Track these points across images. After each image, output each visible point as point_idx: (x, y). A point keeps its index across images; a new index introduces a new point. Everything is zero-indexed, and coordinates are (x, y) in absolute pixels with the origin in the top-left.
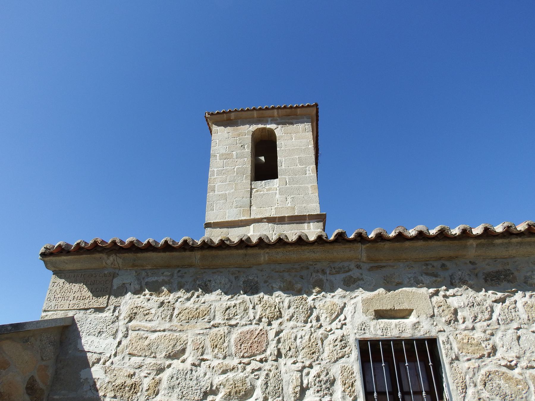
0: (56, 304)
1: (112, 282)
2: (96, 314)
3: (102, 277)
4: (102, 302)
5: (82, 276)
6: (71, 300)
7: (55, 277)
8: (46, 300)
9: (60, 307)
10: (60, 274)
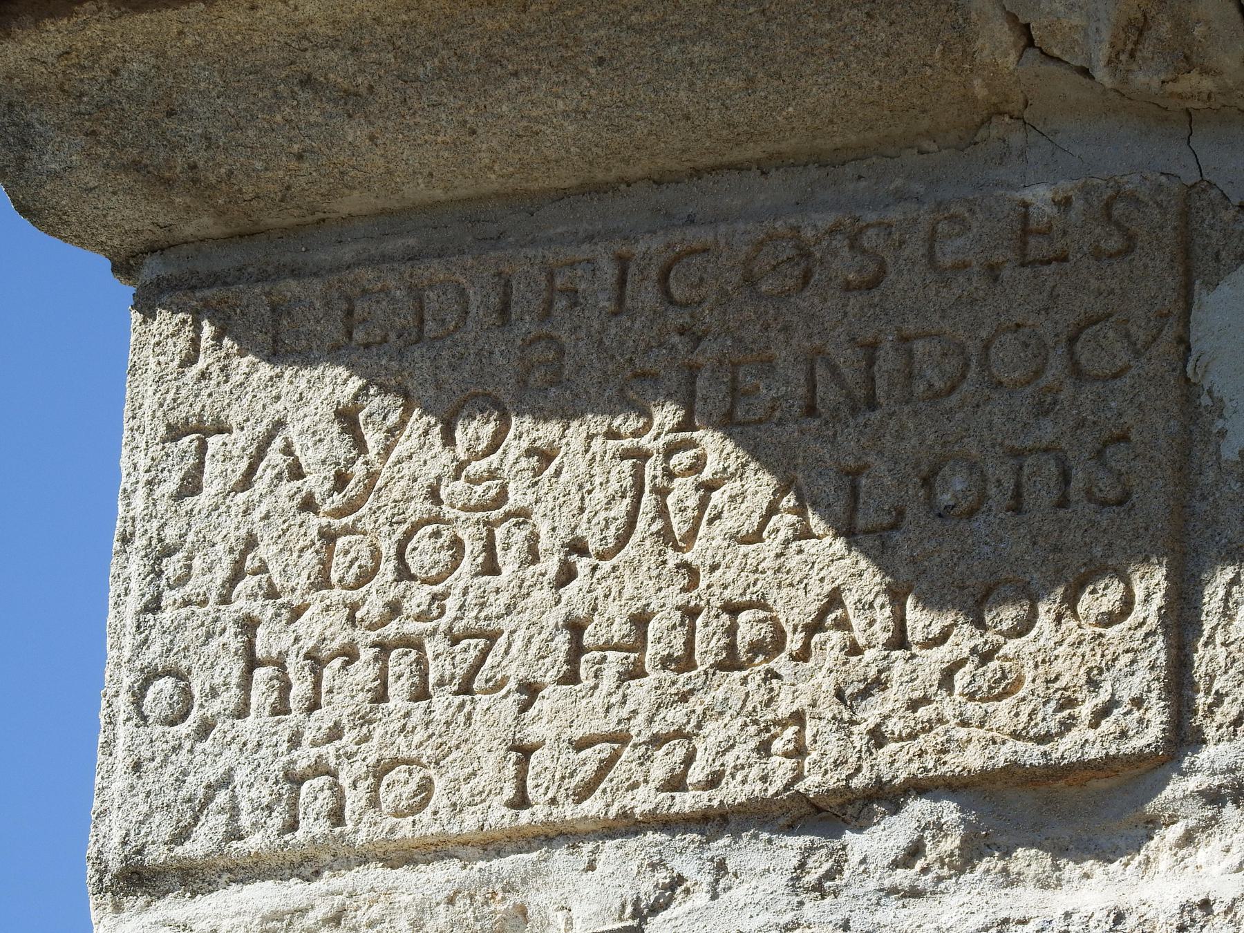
0: (305, 757)
1: (1184, 342)
2: (1009, 880)
3: (993, 272)
4: (1070, 672)
5: (646, 295)
6: (530, 690)
7: (183, 343)
8: (123, 703)
9: (374, 802)
10: (255, 296)
